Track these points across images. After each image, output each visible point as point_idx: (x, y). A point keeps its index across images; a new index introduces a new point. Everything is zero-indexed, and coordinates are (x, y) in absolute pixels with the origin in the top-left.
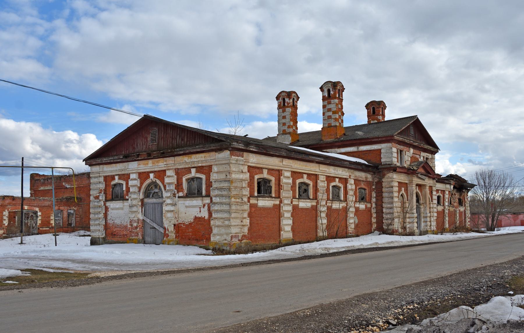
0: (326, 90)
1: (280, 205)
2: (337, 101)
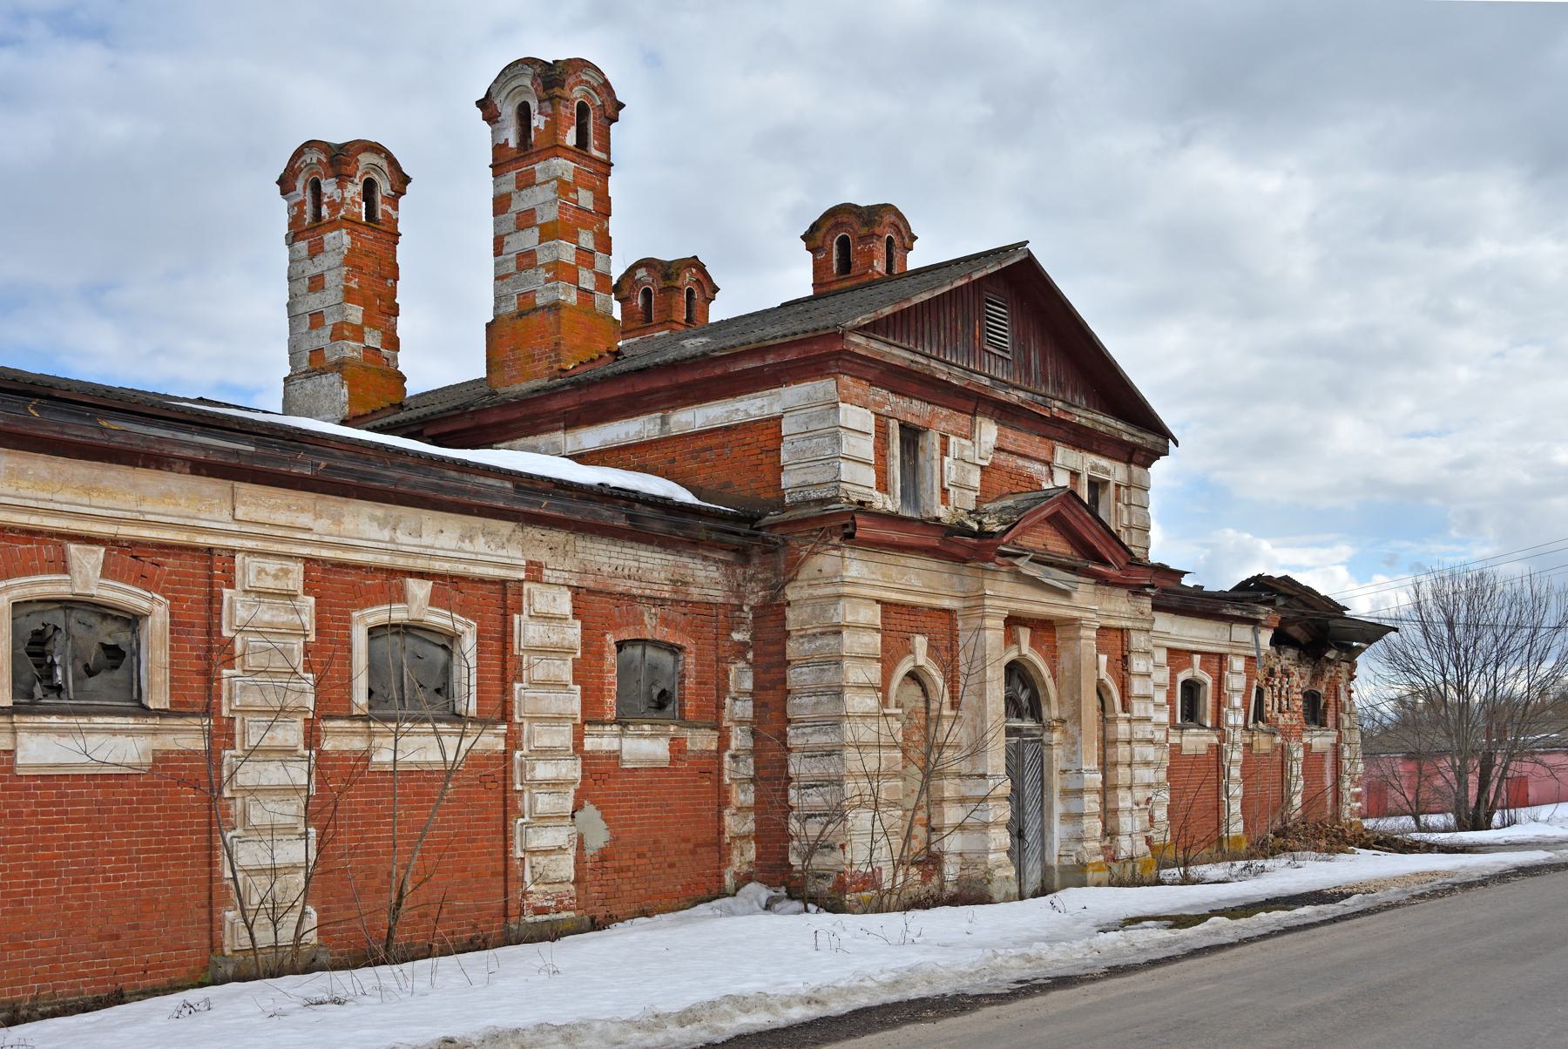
0: (508, 111)
1: (506, 756)
2: (564, 167)
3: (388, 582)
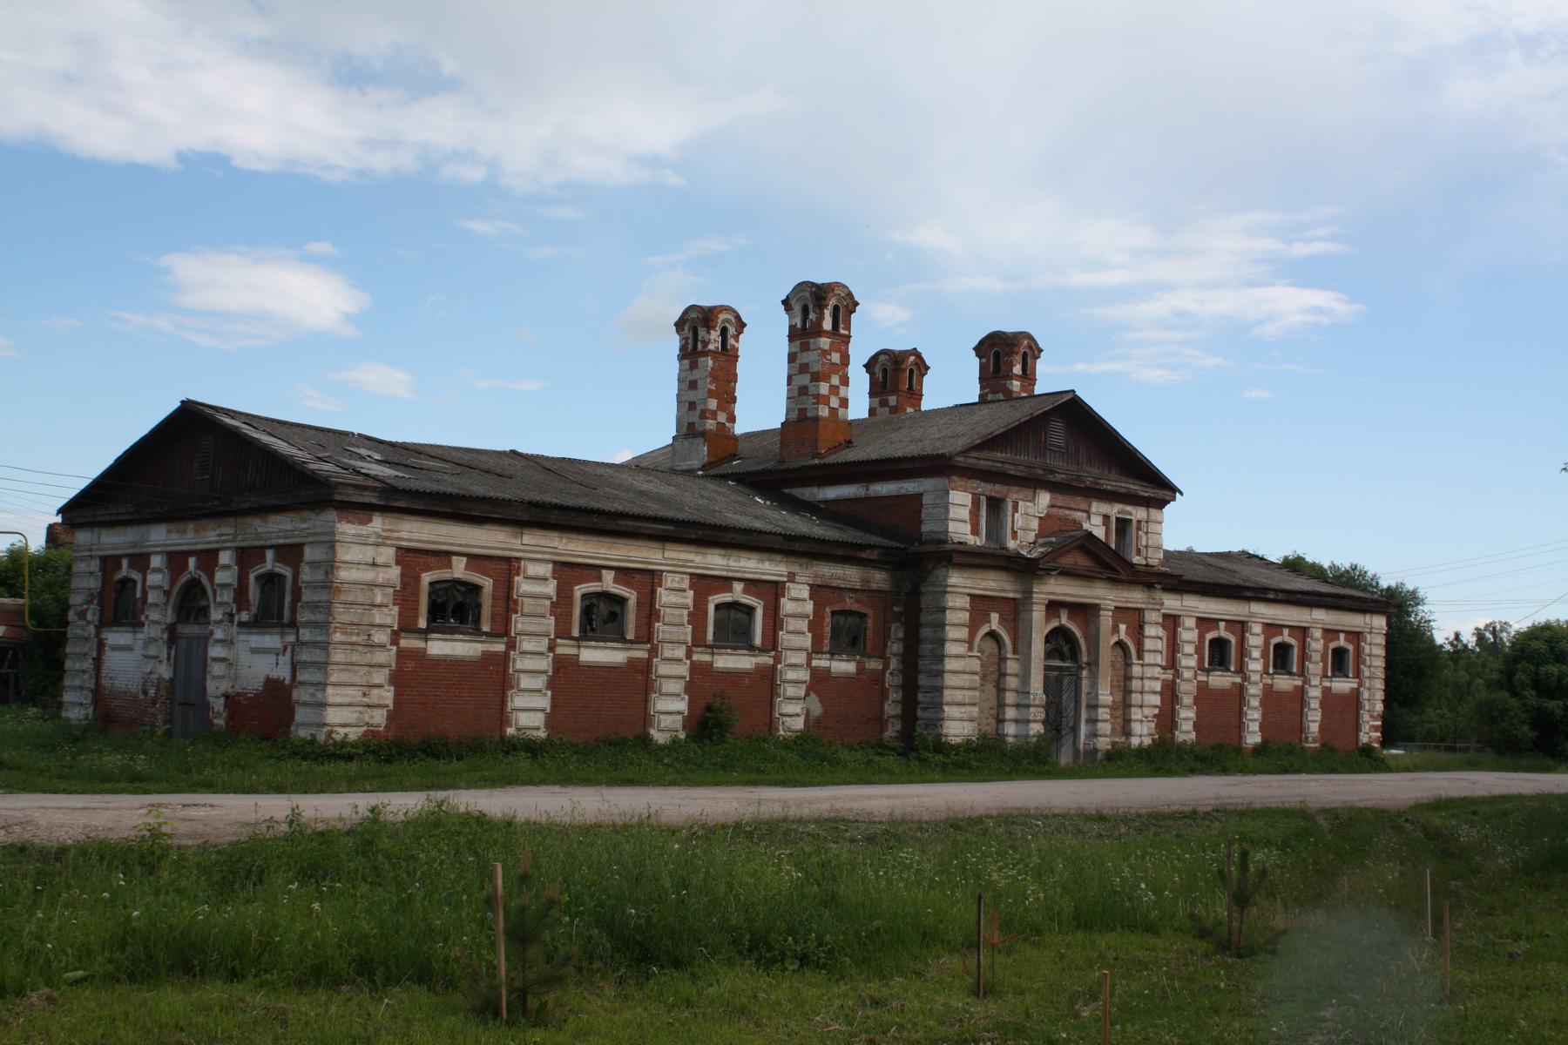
0: (797, 308)
3: (725, 582)
